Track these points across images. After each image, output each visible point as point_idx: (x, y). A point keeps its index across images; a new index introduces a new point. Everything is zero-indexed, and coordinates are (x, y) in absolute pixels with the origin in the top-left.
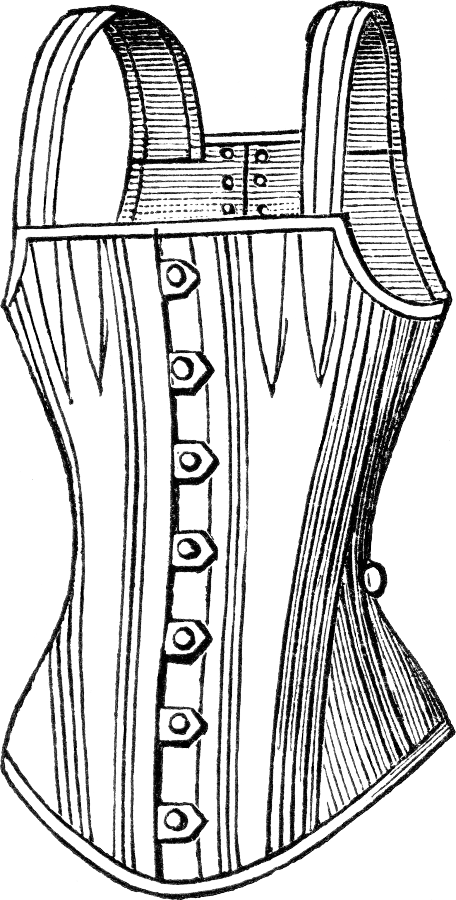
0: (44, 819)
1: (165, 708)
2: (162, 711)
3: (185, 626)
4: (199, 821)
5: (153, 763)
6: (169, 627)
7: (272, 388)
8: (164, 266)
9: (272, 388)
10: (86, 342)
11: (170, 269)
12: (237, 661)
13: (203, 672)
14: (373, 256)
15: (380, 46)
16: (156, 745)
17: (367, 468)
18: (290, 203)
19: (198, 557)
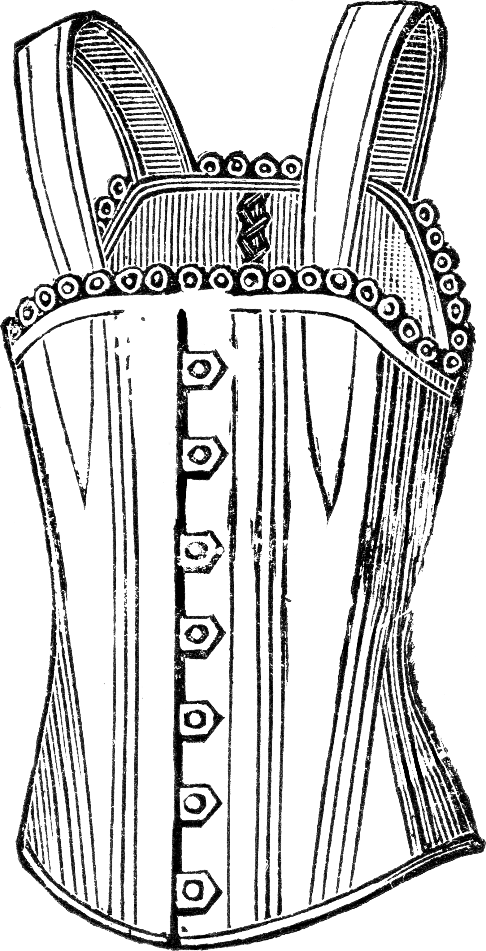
0: (79, 805)
1: (190, 438)
2: (178, 876)
3: (217, 273)
4: (215, 802)
5: (171, 860)
6: (190, 701)
7: (329, 509)
8: (181, 879)
9: (329, 509)
10: (86, 239)
11: (187, 883)
12: (247, 937)
13: (234, 464)
14: (435, 804)
15: (460, 831)
16: (175, 825)
17: (423, 722)
18: (399, 235)
19: (236, 297)
